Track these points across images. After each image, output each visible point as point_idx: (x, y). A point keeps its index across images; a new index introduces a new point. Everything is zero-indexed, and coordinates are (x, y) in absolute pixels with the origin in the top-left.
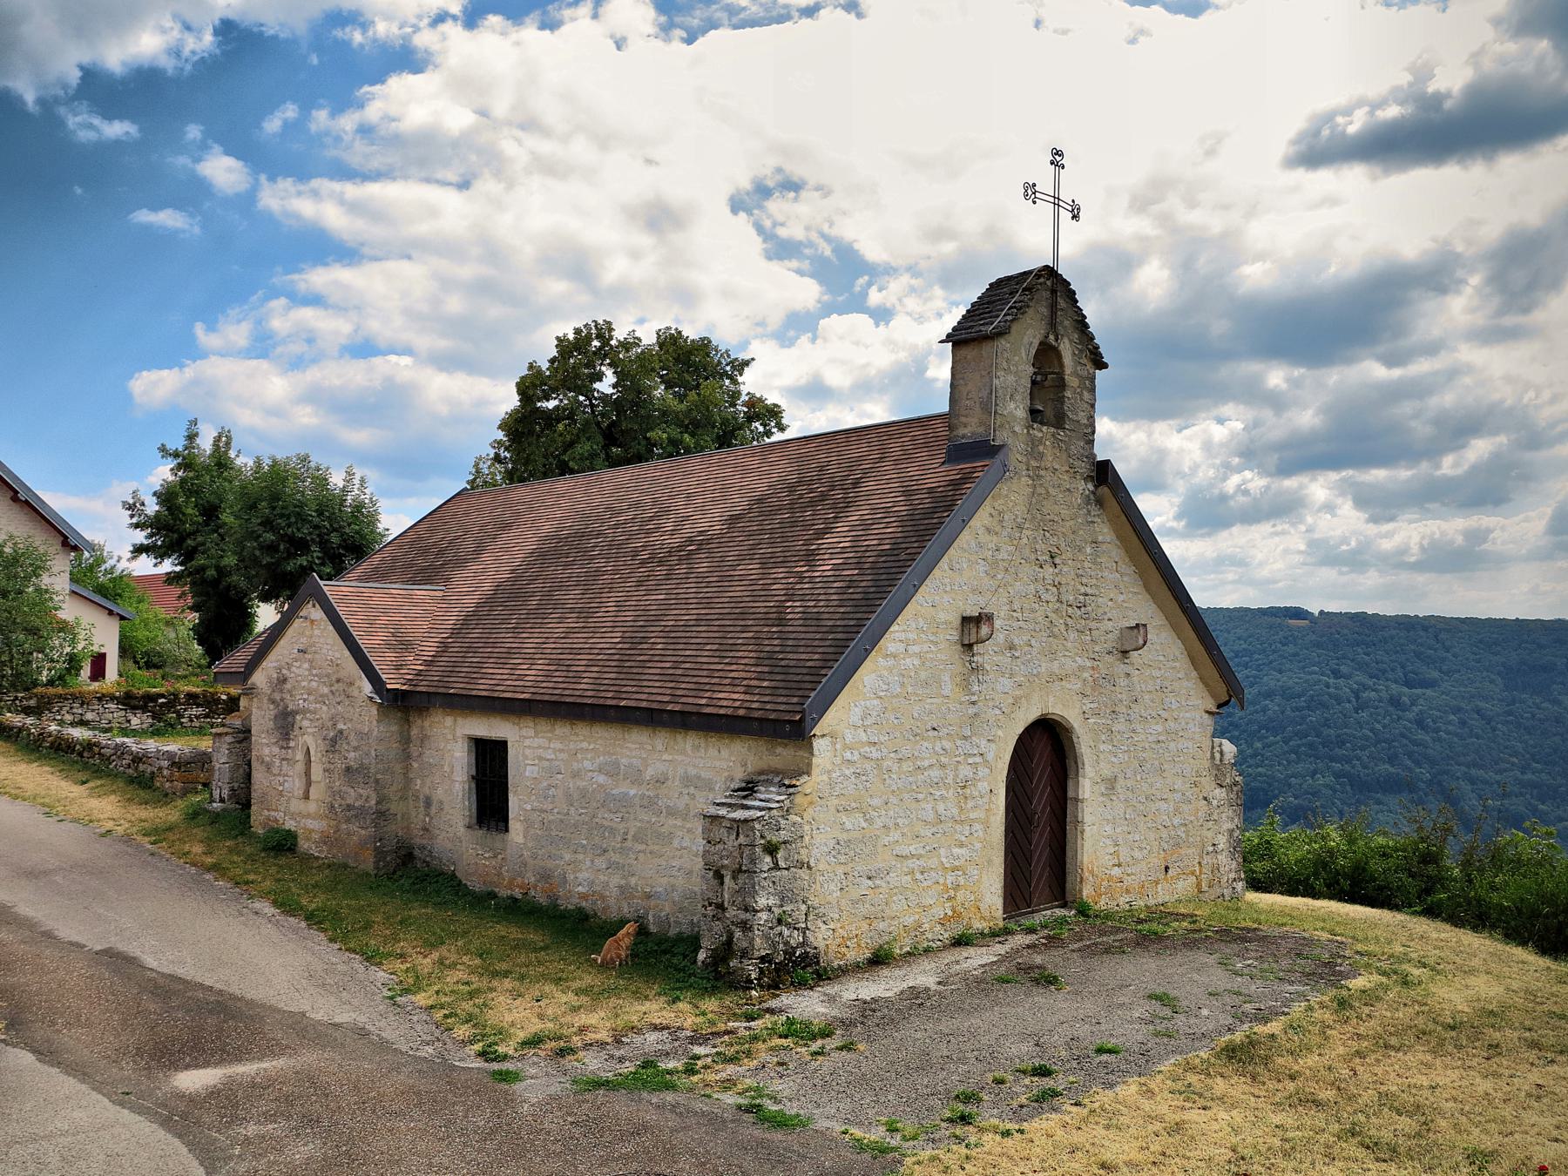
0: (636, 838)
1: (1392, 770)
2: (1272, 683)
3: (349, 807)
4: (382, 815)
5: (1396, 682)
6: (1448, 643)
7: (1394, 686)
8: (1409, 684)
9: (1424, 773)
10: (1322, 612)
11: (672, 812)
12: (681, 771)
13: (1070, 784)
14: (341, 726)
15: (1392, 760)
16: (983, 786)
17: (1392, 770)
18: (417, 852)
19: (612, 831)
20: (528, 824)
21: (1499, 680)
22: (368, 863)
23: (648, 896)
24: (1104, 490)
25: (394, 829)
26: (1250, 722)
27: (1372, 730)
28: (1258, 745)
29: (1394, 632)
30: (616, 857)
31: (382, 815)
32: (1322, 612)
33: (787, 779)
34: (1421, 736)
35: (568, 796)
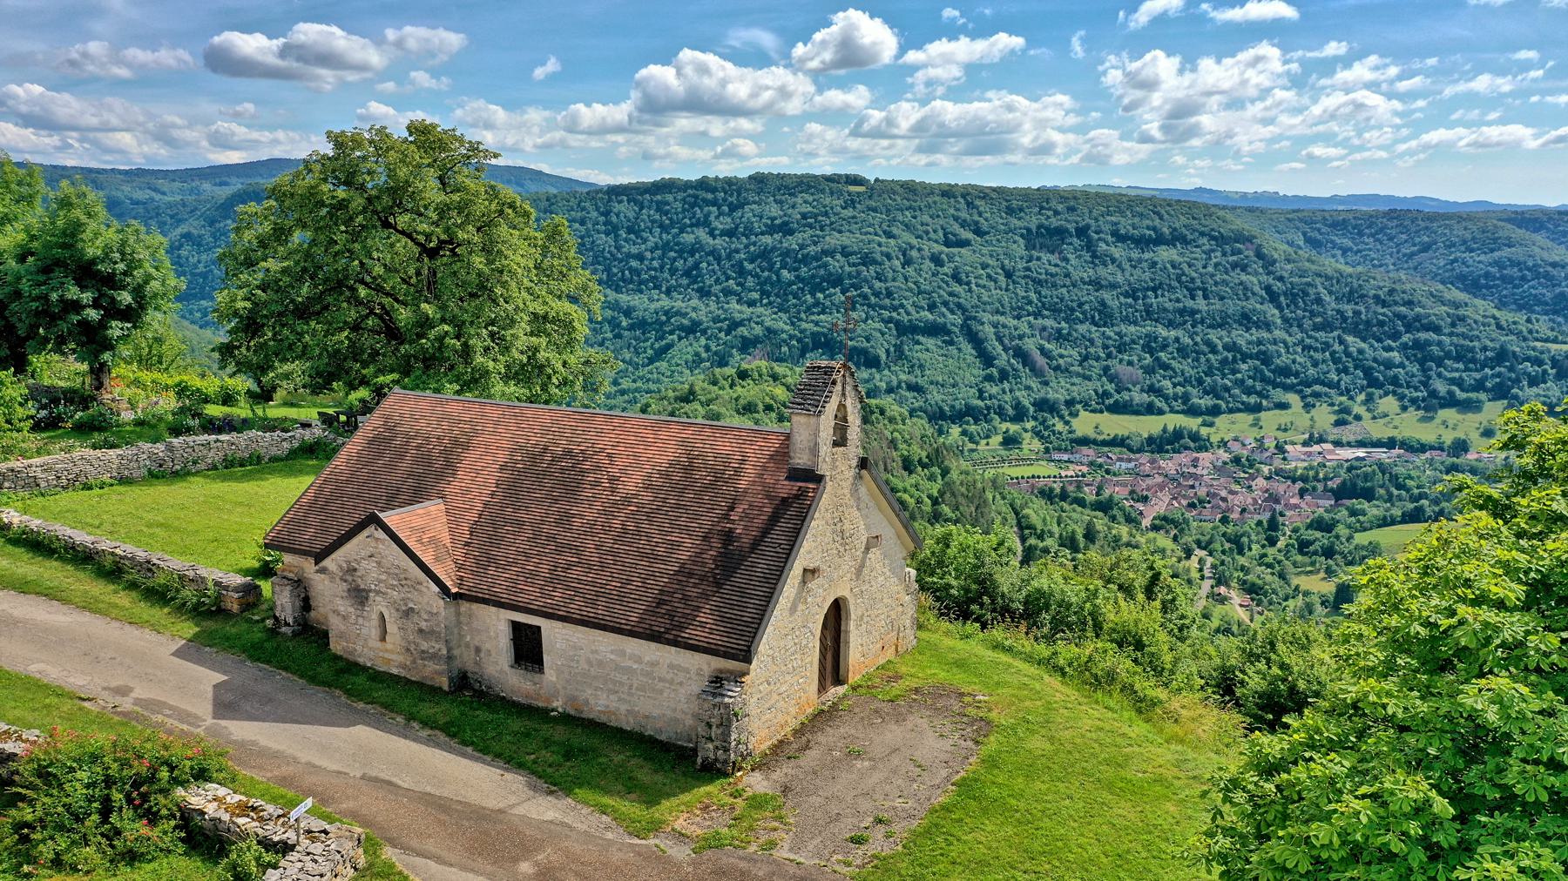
0: (637, 689)
1: (930, 317)
2: (833, 241)
3: (423, 652)
4: (450, 658)
5: (936, 241)
6: (981, 209)
7: (935, 245)
8: (947, 244)
9: (955, 319)
10: (877, 180)
11: (661, 680)
12: (668, 661)
13: (843, 623)
14: (411, 605)
15: (932, 307)
16: (811, 645)
17: (930, 317)
18: (469, 675)
19: (621, 683)
20: (559, 672)
21: (1021, 241)
22: (444, 683)
23: (647, 717)
24: (864, 472)
25: (457, 663)
26: (813, 277)
27: (915, 283)
28: (820, 295)
29: (937, 198)
30: (624, 696)
31: (450, 658)
32: (877, 180)
33: (738, 677)
34: (957, 288)
35: (589, 662)
